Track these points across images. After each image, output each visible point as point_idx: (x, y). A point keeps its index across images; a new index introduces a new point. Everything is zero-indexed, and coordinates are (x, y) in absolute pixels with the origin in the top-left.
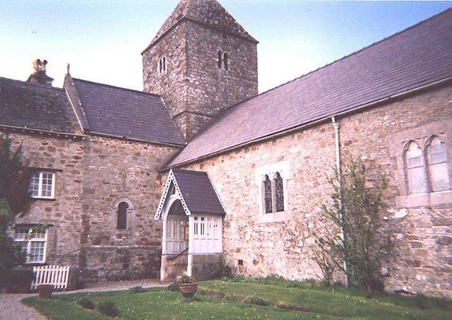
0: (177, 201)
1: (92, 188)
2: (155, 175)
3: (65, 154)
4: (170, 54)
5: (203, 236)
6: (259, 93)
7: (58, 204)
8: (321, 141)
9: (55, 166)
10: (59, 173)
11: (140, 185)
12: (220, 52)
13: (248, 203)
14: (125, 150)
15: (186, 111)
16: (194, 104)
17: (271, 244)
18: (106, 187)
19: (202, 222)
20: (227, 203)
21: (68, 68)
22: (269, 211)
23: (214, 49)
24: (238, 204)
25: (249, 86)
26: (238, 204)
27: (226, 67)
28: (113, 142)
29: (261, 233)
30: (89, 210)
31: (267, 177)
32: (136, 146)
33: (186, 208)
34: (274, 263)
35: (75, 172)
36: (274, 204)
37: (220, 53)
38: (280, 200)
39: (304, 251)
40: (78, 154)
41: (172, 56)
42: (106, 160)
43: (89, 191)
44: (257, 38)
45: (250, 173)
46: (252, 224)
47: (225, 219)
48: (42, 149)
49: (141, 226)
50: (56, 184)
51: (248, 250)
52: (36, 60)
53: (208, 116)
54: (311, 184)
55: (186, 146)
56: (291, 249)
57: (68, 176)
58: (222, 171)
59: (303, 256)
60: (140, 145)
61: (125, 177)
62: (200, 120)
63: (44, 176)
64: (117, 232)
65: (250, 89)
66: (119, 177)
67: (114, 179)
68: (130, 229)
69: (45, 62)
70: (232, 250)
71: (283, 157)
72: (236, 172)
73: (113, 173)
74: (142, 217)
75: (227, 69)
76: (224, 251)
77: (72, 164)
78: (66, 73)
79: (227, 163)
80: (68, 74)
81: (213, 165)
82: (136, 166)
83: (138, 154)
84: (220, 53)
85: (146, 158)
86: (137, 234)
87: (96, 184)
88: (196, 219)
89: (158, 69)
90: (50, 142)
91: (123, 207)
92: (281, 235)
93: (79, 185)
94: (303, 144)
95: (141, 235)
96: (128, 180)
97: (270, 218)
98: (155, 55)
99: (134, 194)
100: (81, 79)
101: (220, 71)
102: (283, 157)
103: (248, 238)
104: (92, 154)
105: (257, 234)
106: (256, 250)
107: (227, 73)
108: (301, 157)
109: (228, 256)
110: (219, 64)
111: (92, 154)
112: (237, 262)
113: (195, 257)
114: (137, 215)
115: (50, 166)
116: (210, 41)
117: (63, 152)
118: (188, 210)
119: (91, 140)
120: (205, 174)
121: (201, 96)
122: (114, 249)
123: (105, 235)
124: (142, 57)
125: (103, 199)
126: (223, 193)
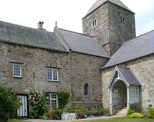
2: (98, 71)
6: (136, 36)
10: (60, 70)
12: (121, 17)
15: (109, 43)
19: (137, 90)
25: (132, 33)
27: (124, 24)
32: (90, 58)
35: (67, 69)
41: (100, 19)
42: (79, 64)
43: (72, 78)
48: (52, 58)
49: (94, 94)
52: (39, 22)
61: (86, 72)
63: (54, 71)
65: (133, 34)
66: (84, 72)
69: (43, 23)
72: (147, 66)
77: (65, 65)
79: (143, 64)
80: (56, 26)
83: (91, 62)
85: (95, 63)
86: (93, 97)
89: (92, 25)
91: (86, 85)
96: (87, 73)
104: (73, 61)
107: (124, 26)
114: (93, 89)
118: (128, 84)
121: (115, 36)
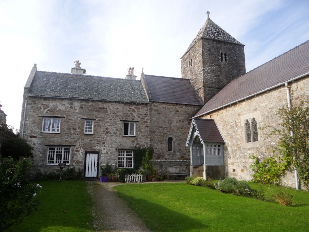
0: (197, 136)
1: (154, 130)
3: (140, 113)
4: (195, 57)
5: (212, 156)
7: (138, 139)
8: (279, 98)
9: (135, 120)
10: (137, 123)
11: (179, 128)
13: (238, 136)
18: (161, 129)
20: (226, 136)
21: (143, 70)
22: (249, 140)
23: (218, 52)
26: (232, 137)
28: (164, 106)
29: (245, 154)
30: (153, 141)
31: (247, 121)
33: (201, 140)
35: (146, 122)
36: (252, 137)
37: (222, 54)
38: (256, 134)
40: (146, 112)
41: (195, 58)
43: (152, 132)
44: (244, 44)
46: (240, 148)
48: (129, 111)
49: (180, 150)
50: (136, 128)
55: (203, 105)
57: (142, 124)
60: (178, 106)
61: (171, 124)
62: (211, 91)
66: (168, 124)
69: (133, 68)
71: (257, 109)
74: (181, 145)
75: (226, 62)
77: (144, 118)
78: (142, 72)
80: (143, 73)
81: (217, 115)
82: (177, 118)
83: (178, 111)
85: (182, 113)
86: (178, 154)
87: (156, 128)
89: (189, 65)
90: (133, 107)
91: (170, 140)
93: (148, 129)
95: (180, 155)
96: (172, 125)
97: (250, 145)
98: (187, 59)
99: (176, 133)
100: (153, 75)
102: (257, 109)
103: (238, 156)
104: (153, 112)
105: (243, 155)
108: (268, 108)
111: (153, 112)
112: (232, 171)
114: (178, 144)
115: (133, 119)
116: (216, 48)
117: (139, 112)
119: (153, 105)
122: (166, 162)
125: (160, 136)
126: (223, 131)
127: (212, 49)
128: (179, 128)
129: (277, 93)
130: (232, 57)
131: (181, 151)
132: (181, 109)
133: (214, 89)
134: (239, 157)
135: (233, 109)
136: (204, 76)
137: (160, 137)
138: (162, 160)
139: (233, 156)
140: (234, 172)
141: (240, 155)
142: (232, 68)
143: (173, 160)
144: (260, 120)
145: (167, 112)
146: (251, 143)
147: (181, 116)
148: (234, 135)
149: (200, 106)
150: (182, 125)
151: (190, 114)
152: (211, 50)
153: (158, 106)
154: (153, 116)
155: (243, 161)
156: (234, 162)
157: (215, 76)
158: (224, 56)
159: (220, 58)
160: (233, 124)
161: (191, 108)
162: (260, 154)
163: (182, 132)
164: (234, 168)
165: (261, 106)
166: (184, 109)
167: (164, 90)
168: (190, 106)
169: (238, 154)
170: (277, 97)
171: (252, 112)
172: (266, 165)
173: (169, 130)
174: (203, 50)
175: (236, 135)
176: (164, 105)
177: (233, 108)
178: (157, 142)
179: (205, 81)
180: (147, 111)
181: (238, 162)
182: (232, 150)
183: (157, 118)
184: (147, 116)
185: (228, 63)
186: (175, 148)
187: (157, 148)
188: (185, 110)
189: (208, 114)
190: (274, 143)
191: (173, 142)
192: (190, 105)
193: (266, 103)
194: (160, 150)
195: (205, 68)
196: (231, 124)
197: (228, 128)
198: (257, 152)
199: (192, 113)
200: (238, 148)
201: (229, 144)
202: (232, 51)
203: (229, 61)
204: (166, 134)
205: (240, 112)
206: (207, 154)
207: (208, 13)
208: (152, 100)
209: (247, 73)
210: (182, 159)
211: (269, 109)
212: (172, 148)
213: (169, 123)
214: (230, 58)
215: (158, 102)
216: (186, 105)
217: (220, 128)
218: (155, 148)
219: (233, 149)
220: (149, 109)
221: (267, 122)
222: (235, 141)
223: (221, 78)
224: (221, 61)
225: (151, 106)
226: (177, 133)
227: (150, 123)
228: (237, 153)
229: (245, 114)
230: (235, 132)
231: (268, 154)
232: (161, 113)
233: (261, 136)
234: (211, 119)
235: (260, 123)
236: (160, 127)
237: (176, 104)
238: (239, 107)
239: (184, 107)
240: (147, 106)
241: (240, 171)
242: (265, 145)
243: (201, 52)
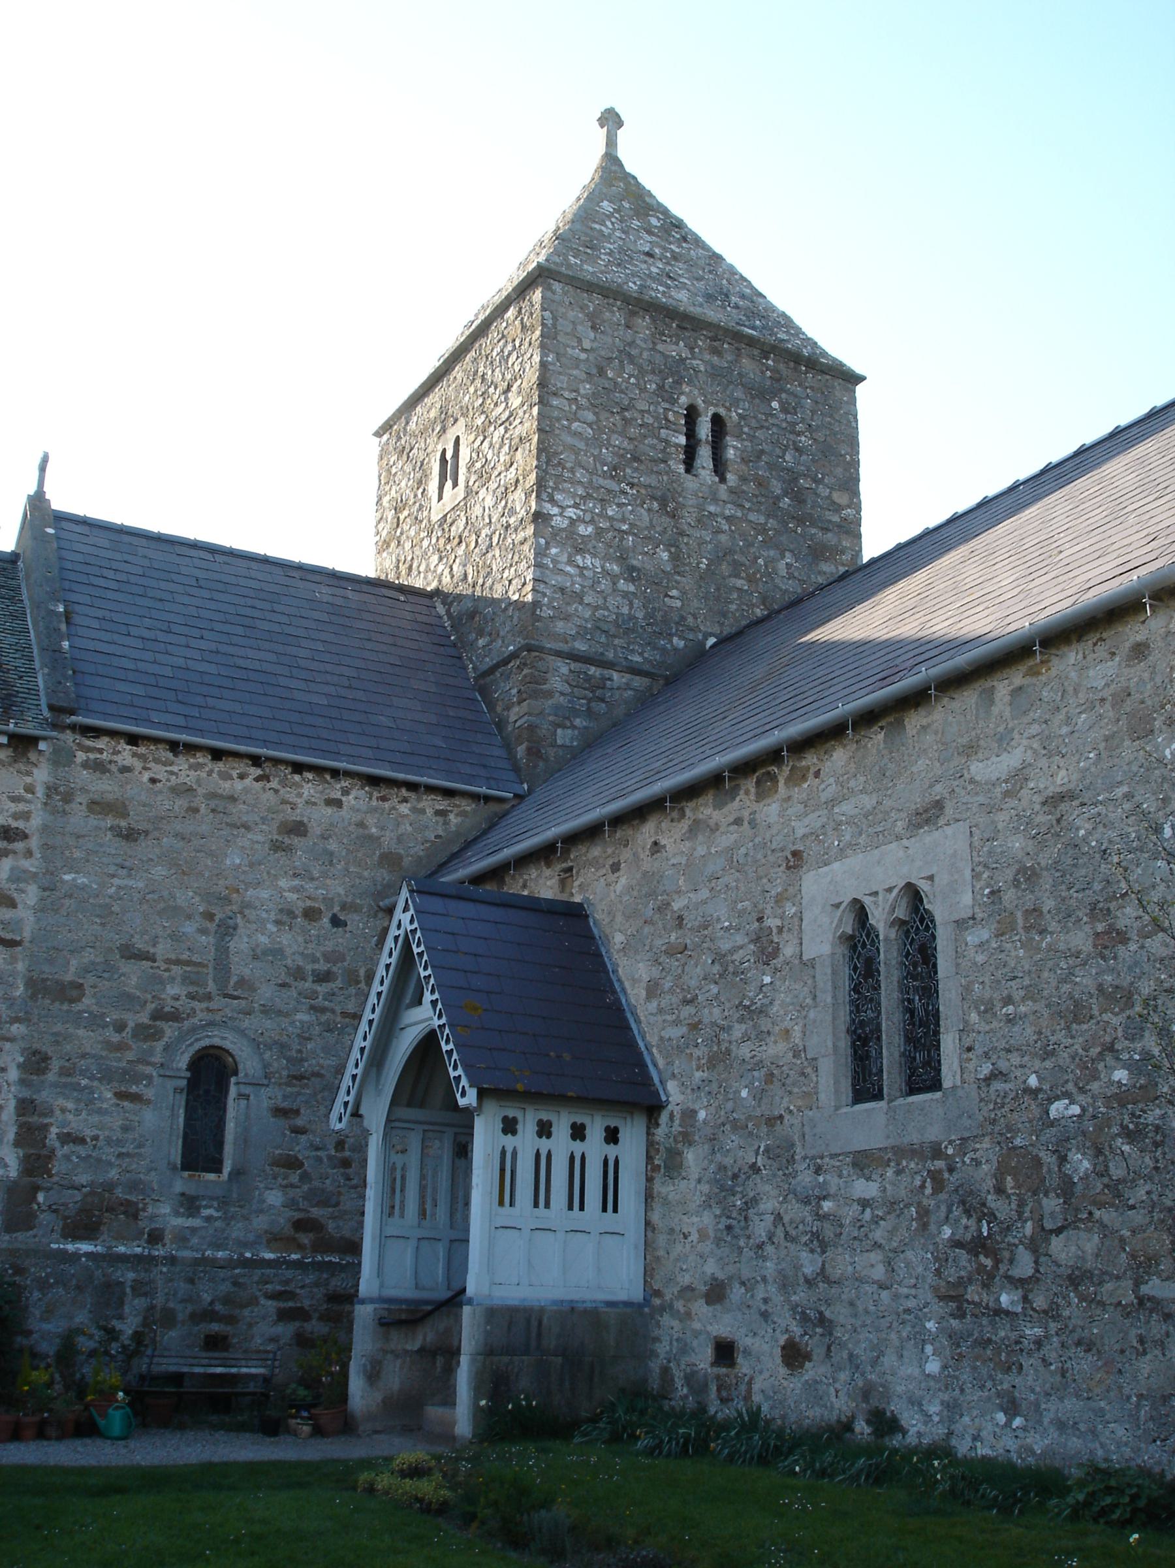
1: (69, 977)
8: (1128, 706)
11: (298, 974)
13: (775, 1049)
14: (239, 811)
16: (567, 618)
17: (874, 1266)
18: (133, 975)
21: (43, 469)
23: (666, 395)
24: (719, 1059)
25: (818, 553)
26: (719, 1059)
27: (719, 467)
28: (183, 769)
29: (827, 1205)
30: (51, 1076)
31: (860, 912)
32: (289, 794)
34: (889, 1360)
37: (692, 415)
39: (1040, 1302)
40: (16, 816)
42: (144, 848)
44: (858, 370)
45: (780, 900)
47: (660, 1133)
49: (292, 1163)
51: (760, 1293)
53: (635, 671)
54: (1080, 939)
56: (973, 1293)
58: (652, 894)
59: (1033, 1331)
60: (309, 788)
61: (227, 930)
64: (179, 1186)
66: (203, 931)
67: (175, 937)
68: (237, 1174)
70: (687, 1291)
71: (939, 805)
73: (173, 911)
74: (299, 1122)
75: (723, 479)
76: (652, 1293)
78: (32, 489)
81: (615, 868)
82: (283, 883)
83: (298, 829)
84: (692, 415)
85: (333, 845)
86: (274, 1198)
87: (88, 956)
88: (510, 1127)
92: (924, 1213)
93: (13, 960)
94: (1035, 729)
95: (291, 1204)
96: (239, 944)
99: (266, 1011)
101: (690, 482)
102: (939, 805)
103: (760, 1228)
104: (78, 817)
105: (806, 1212)
106: (800, 1296)
108: (1028, 799)
109: (666, 1320)
110: (689, 462)
111: (78, 817)
113: (493, 1313)
119: (81, 756)
120: (576, 914)
121: (605, 584)
123: (119, 1192)
124: (374, 445)
125: (120, 1027)
126: (653, 1006)
127: (622, 367)
128: (299, 969)
129: (1111, 668)
130: (765, 446)
131: (294, 1178)
132: (329, 811)
133: (615, 676)
134: (771, 1237)
135: (746, 814)
136: (537, 565)
137: (116, 1038)
138: (122, 1249)
139: (724, 1221)
140: (724, 1370)
141: (786, 1219)
142: (764, 531)
143: (218, 1247)
144: (967, 899)
145: (204, 828)
146: (882, 1104)
147: (325, 875)
148: (746, 1038)
149: (487, 799)
150: (329, 946)
151: (406, 862)
152: (610, 374)
153: (126, 769)
154: (77, 854)
155: (808, 1270)
156: (730, 1278)
157: (632, 573)
158: (704, 429)
159: (677, 445)
160: (740, 939)
161: (414, 810)
162: (950, 1211)
163: (323, 1010)
164: (724, 1325)
165: (972, 781)
166: (357, 818)
167: (203, 645)
168: (404, 792)
169: (768, 1205)
170: (1108, 706)
171: (899, 838)
172: (63, 1144)
173: (211, 987)
174: (543, 365)
175: (762, 1036)
176: (182, 764)
177: (745, 800)
178: (84, 1082)
179: (550, 606)
180: (21, 807)
181: (764, 1279)
182: (722, 1168)
183: (112, 869)
184: (19, 846)
185: (732, 491)
186: (244, 1141)
187: (81, 1141)
188: (361, 825)
189: (545, 853)
190: (1076, 1110)
191: (233, 1091)
192: (412, 787)
193: (1010, 761)
194: (108, 1153)
195: (552, 500)
196: (725, 946)
197: (694, 974)
198: (928, 1191)
199: (419, 850)
200: (767, 1150)
201: (694, 1113)
202: (769, 401)
203: (743, 479)
204: (175, 1016)
205: (800, 832)
206: (501, 1203)
207: (611, 120)
208: (72, 712)
209: (873, 561)
210: (300, 1247)
211: (1044, 804)
212: (220, 1144)
213: (212, 927)
214: (749, 458)
215: (133, 739)
216: (374, 781)
217: (635, 981)
218: (67, 1138)
219: (728, 1161)
220: (40, 792)
221: (1020, 922)
222: (744, 1093)
223: (674, 593)
224: (681, 468)
225: (62, 758)
226: (280, 1013)
227: (41, 909)
228: (755, 1201)
229: (842, 853)
230: (751, 1012)
231: (1022, 1204)
232: (147, 833)
233: (967, 1042)
234: (564, 897)
235: (961, 925)
236: (131, 954)
237: (286, 762)
238: (799, 793)
239: (357, 798)
240: (29, 762)
241: (773, 1362)
242: (994, 1122)
243: (532, 376)
